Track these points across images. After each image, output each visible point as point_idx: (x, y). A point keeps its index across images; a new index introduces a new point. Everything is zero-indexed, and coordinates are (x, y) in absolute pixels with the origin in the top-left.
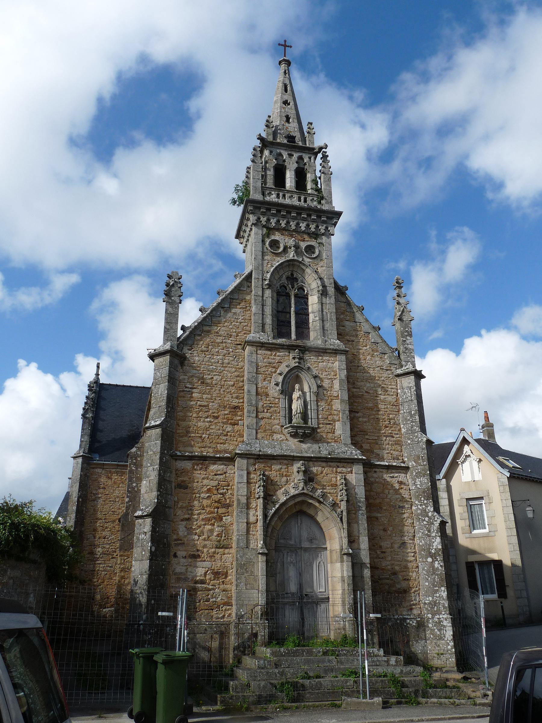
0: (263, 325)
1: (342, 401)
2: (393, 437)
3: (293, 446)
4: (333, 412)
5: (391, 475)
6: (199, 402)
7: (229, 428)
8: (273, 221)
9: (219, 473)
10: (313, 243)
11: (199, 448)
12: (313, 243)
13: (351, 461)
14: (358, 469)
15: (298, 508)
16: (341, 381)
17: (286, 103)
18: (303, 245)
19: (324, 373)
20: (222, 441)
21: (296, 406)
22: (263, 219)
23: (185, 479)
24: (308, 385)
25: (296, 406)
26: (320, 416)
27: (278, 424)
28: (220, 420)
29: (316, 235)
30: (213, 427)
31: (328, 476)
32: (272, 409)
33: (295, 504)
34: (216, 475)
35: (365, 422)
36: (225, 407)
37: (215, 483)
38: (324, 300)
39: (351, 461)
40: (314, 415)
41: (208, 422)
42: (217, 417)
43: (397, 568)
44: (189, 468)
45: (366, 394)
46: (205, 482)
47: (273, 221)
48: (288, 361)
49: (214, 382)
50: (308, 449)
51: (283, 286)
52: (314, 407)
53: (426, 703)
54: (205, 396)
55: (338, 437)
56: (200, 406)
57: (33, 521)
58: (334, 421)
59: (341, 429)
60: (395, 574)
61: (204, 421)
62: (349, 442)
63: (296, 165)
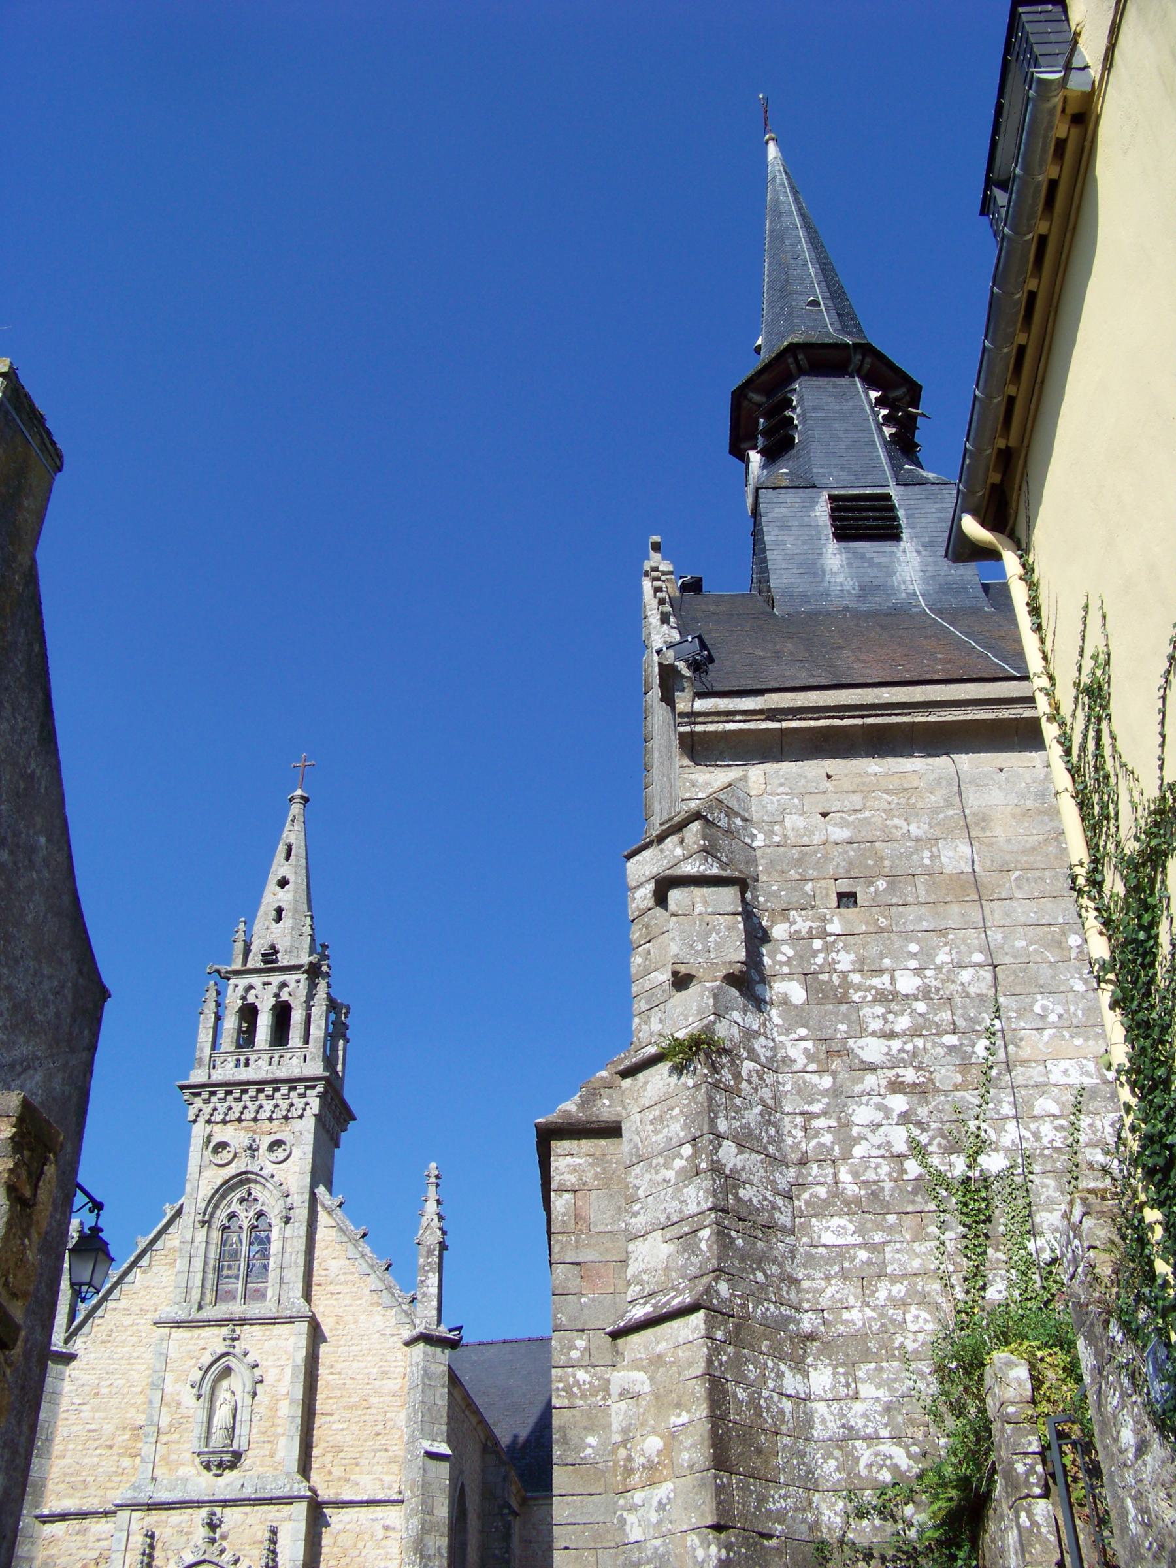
1: (292, 1402)
2: (386, 1450)
3: (205, 1484)
4: (277, 1421)
5: (374, 1516)
6: (88, 1427)
9: (103, 1536)
11: (81, 1498)
19: (272, 1358)
20: (113, 1485)
21: (222, 1416)
23: (51, 1552)
24: (238, 1383)
25: (222, 1416)
26: (254, 1431)
27: (188, 1450)
28: (115, 1450)
30: (104, 1463)
32: (183, 1426)
34: (98, 1540)
35: (342, 1430)
36: (124, 1428)
37: (95, 1554)
38: (321, 1190)
39: (288, 1500)
40: (245, 1431)
41: (97, 1456)
42: (111, 1447)
44: (61, 1533)
45: (351, 1382)
46: (83, 1553)
48: (213, 1340)
49: (114, 1391)
50: (227, 1484)
52: (247, 1417)
54: (98, 1415)
55: (271, 1459)
56: (89, 1431)
61: (91, 1456)
63: (273, 1001)
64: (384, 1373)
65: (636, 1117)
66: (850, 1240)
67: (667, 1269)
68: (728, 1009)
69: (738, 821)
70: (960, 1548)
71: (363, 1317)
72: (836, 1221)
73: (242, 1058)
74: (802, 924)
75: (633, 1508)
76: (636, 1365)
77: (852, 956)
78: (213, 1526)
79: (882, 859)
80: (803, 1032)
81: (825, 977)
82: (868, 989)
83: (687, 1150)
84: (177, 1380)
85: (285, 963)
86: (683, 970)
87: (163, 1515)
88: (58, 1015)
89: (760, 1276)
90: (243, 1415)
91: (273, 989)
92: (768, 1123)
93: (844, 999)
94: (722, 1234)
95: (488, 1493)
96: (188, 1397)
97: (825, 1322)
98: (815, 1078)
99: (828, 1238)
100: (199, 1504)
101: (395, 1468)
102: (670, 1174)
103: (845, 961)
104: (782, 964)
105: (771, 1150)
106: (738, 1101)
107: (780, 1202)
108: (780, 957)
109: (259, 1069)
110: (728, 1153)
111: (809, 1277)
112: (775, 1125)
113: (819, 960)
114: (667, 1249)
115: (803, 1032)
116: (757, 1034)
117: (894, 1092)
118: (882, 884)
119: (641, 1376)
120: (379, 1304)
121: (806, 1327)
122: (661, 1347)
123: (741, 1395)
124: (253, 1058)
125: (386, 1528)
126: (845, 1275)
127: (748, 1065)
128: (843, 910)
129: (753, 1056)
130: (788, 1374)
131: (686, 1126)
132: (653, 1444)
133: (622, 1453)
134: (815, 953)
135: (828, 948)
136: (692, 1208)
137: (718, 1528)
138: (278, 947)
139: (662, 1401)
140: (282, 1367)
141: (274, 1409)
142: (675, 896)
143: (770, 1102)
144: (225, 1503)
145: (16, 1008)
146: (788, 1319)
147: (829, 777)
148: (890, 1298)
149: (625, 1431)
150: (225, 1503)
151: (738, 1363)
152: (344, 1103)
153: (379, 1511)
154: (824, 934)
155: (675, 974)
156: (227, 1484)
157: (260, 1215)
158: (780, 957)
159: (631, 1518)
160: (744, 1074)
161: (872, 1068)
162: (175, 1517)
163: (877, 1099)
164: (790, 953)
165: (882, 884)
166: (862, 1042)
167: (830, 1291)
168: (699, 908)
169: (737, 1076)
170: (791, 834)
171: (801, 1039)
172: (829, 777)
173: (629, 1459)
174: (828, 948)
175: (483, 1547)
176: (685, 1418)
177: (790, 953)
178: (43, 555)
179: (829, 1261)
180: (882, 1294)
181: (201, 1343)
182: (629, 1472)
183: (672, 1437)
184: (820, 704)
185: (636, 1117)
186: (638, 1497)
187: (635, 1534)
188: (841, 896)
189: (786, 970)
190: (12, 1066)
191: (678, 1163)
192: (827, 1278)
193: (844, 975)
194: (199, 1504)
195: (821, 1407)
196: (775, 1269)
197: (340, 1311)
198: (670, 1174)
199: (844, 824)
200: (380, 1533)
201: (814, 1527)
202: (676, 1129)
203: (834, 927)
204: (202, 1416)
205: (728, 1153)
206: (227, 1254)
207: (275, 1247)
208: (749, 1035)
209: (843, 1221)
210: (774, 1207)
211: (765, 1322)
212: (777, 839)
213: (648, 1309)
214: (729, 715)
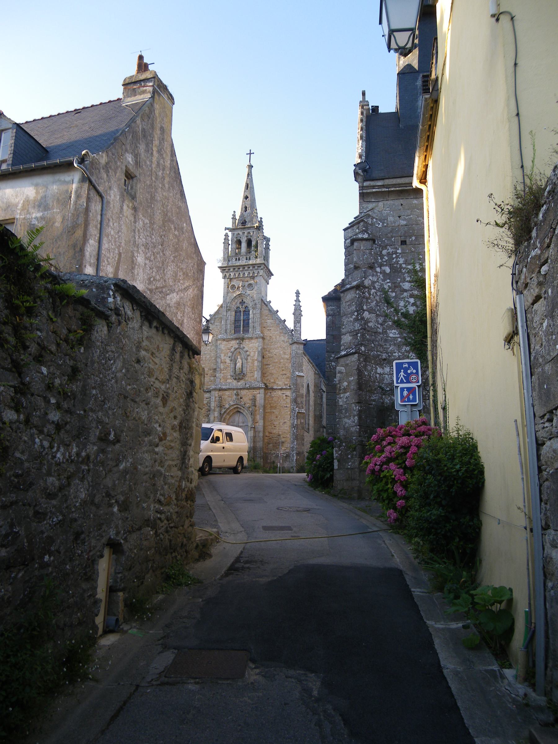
0: (226, 330)
7: (212, 378)
8: (232, 274)
10: (252, 282)
12: (252, 282)
13: (259, 388)
14: (262, 391)
15: (236, 410)
16: (259, 352)
17: (246, 198)
18: (247, 284)
22: (227, 275)
29: (253, 278)
31: (247, 395)
33: (235, 408)
39: (259, 388)
43: (280, 433)
47: (232, 274)
50: (241, 384)
51: (238, 308)
53: (535, 623)
57: (180, 457)
58: (254, 371)
59: (257, 375)
60: (279, 435)
62: (260, 380)
63: (246, 239)
64: (285, 353)
65: (344, 304)
66: (397, 336)
67: (350, 343)
68: (368, 276)
69: (375, 220)
70: (81, 467)
71: (278, 337)
72: (393, 331)
73: (237, 258)
74: (390, 250)
75: (341, 398)
76: (342, 366)
77: (403, 259)
78: (237, 395)
79: (414, 230)
80: (388, 281)
81: (396, 265)
82: (407, 269)
83: (356, 314)
84: (225, 356)
85: (249, 226)
86: (357, 265)
87: (224, 392)
88: (194, 273)
89: (373, 345)
90: (245, 365)
91: (246, 234)
92: (378, 306)
93: (401, 271)
94: (363, 335)
95: (316, 386)
96: (228, 361)
97: (389, 356)
98: (391, 293)
99: (391, 335)
100: (234, 389)
101: (288, 380)
102: (352, 319)
103: (401, 261)
104: (384, 262)
105: (378, 313)
106: (369, 301)
107: (379, 326)
108: (384, 260)
109: (243, 262)
110: (366, 315)
111: (385, 345)
112: (379, 306)
113: (394, 261)
114: (350, 338)
115: (388, 281)
116: (376, 282)
117: (411, 297)
118: (413, 238)
119: (343, 368)
120: (283, 333)
121: (384, 357)
122: (348, 362)
123: (366, 373)
124: (241, 258)
125: (286, 396)
126: (395, 344)
127: (373, 291)
128: (402, 246)
129: (374, 288)
130: (379, 368)
131: (356, 308)
132: (345, 384)
133: (338, 386)
134: (393, 259)
135: (397, 257)
136: (357, 328)
137: (358, 403)
138: (247, 220)
139: (348, 375)
140: (255, 352)
141: (253, 363)
142: (356, 244)
143: (378, 300)
144: (241, 389)
145: (184, 274)
146: (380, 355)
147: (402, 205)
148: (405, 350)
149: (339, 381)
150: (241, 389)
151: (365, 366)
152: (269, 271)
153: (284, 392)
154: (396, 253)
155: (355, 266)
156: (241, 384)
157: (246, 307)
158: (384, 260)
159: (340, 400)
160: (372, 293)
161: (406, 291)
162: (227, 393)
163: (406, 299)
164: (387, 258)
165: (413, 238)
166: (404, 284)
167: (391, 348)
168: (362, 248)
169: (370, 294)
170: (389, 223)
171: (388, 283)
172: (402, 205)
173: (340, 387)
174: (397, 257)
175: (315, 401)
176: (352, 378)
177: (387, 258)
178: (174, 136)
179: (391, 341)
180: (403, 350)
181: (231, 345)
182: (340, 390)
183: (349, 383)
184: (400, 183)
185: (344, 304)
186: (342, 395)
187: (341, 403)
188: (402, 242)
189: (385, 263)
190: (185, 289)
191: (354, 317)
192: (390, 345)
193: (401, 264)
194: (234, 389)
195: (386, 376)
196: (377, 343)
197: (271, 335)
198: (352, 319)
199: (405, 220)
200: (285, 398)
201: (383, 403)
202: (353, 308)
203: (399, 251)
204: (232, 366)
205: (366, 315)
206: (237, 321)
207: (251, 316)
208: (373, 282)
209: (395, 331)
210: (378, 327)
211: (373, 356)
212: (385, 224)
213: (345, 352)
214: (373, 187)
